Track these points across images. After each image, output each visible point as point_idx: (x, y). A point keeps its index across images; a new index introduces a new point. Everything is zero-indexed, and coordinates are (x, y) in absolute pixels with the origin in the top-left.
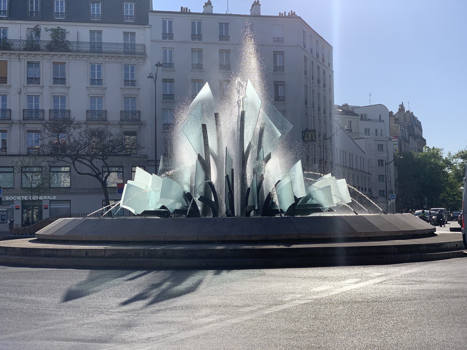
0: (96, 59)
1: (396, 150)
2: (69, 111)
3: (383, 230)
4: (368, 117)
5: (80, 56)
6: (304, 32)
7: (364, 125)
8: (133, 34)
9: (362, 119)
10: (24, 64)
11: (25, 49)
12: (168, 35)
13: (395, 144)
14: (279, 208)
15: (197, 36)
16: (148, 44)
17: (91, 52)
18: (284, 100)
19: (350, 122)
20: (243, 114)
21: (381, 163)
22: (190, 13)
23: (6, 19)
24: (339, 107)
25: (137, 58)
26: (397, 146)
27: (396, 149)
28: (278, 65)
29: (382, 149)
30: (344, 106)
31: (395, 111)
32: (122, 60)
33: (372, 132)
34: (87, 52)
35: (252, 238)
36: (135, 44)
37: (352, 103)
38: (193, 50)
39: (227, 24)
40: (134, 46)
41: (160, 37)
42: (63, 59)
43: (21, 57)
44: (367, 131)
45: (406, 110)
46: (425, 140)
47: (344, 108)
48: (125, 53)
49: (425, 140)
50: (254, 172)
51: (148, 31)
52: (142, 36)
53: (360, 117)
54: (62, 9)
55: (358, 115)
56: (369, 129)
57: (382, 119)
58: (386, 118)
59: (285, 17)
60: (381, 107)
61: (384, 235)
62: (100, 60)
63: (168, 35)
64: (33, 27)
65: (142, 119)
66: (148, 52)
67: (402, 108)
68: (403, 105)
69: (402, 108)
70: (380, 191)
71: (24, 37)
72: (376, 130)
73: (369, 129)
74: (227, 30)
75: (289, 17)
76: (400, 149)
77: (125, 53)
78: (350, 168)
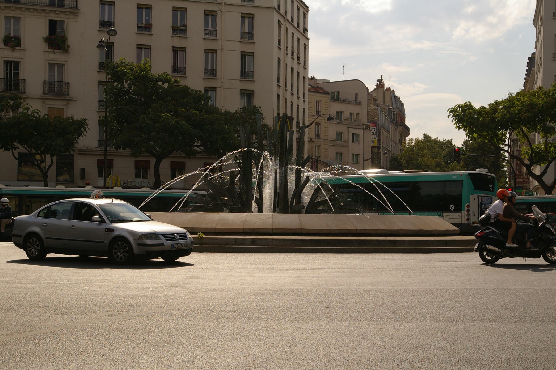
0: (13, 12)
1: (373, 141)
5: (23, 10)
7: (335, 108)
13: (373, 134)
14: (229, 101)
19: (318, 102)
20: (8, 262)
25: (67, 13)
26: (375, 136)
27: (374, 139)
31: (371, 87)
32: (47, 15)
45: (386, 87)
46: (409, 129)
49: (408, 129)
50: (244, 23)
53: (330, 96)
57: (359, 99)
58: (363, 98)
60: (358, 84)
62: (18, 14)
67: (380, 84)
68: (382, 80)
69: (380, 84)
70: (253, 53)
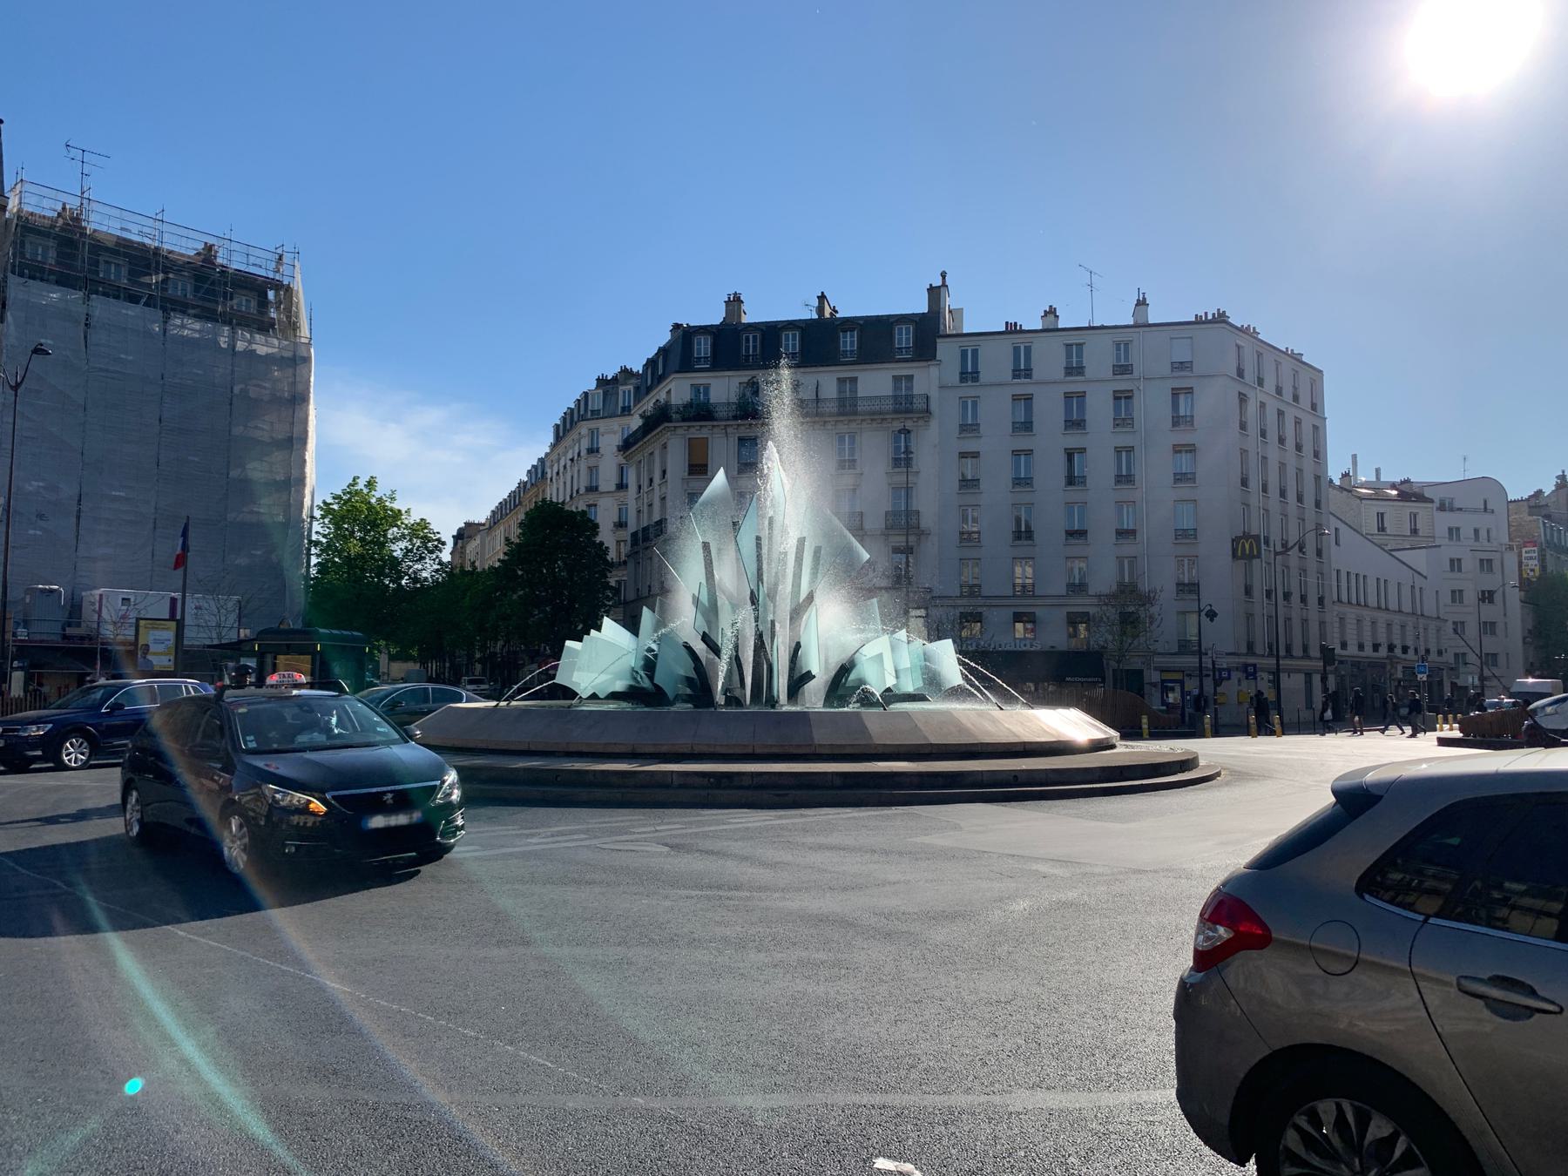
2: (918, 512)
3: (934, 741)
4: (1457, 505)
6: (1238, 347)
7: (1445, 520)
8: (910, 378)
9: (1442, 508)
10: (733, 441)
11: (735, 418)
12: (969, 375)
15: (1022, 372)
16: (934, 394)
17: (840, 414)
18: (1084, 483)
19: (1414, 517)
21: (1457, 595)
22: (1022, 331)
23: (912, 360)
24: (1393, 486)
28: (1182, 413)
29: (1491, 570)
30: (1402, 483)
33: (1466, 532)
34: (831, 415)
35: (610, 750)
36: (912, 396)
37: (1420, 474)
38: (1016, 398)
39: (1080, 345)
40: (910, 398)
41: (955, 378)
42: (704, 433)
43: (730, 430)
44: (1453, 532)
47: (1403, 488)
48: (896, 411)
51: (934, 371)
52: (927, 380)
54: (755, 347)
55: (1432, 501)
56: (1458, 529)
59: (1207, 322)
60: (1490, 485)
61: (881, 751)
63: (969, 375)
64: (746, 379)
65: (923, 525)
66: (934, 406)
71: (734, 399)
72: (1476, 531)
73: (1458, 529)
74: (1080, 355)
75: (1214, 321)
76: (1543, 568)
77: (896, 411)
78: (1379, 608)
